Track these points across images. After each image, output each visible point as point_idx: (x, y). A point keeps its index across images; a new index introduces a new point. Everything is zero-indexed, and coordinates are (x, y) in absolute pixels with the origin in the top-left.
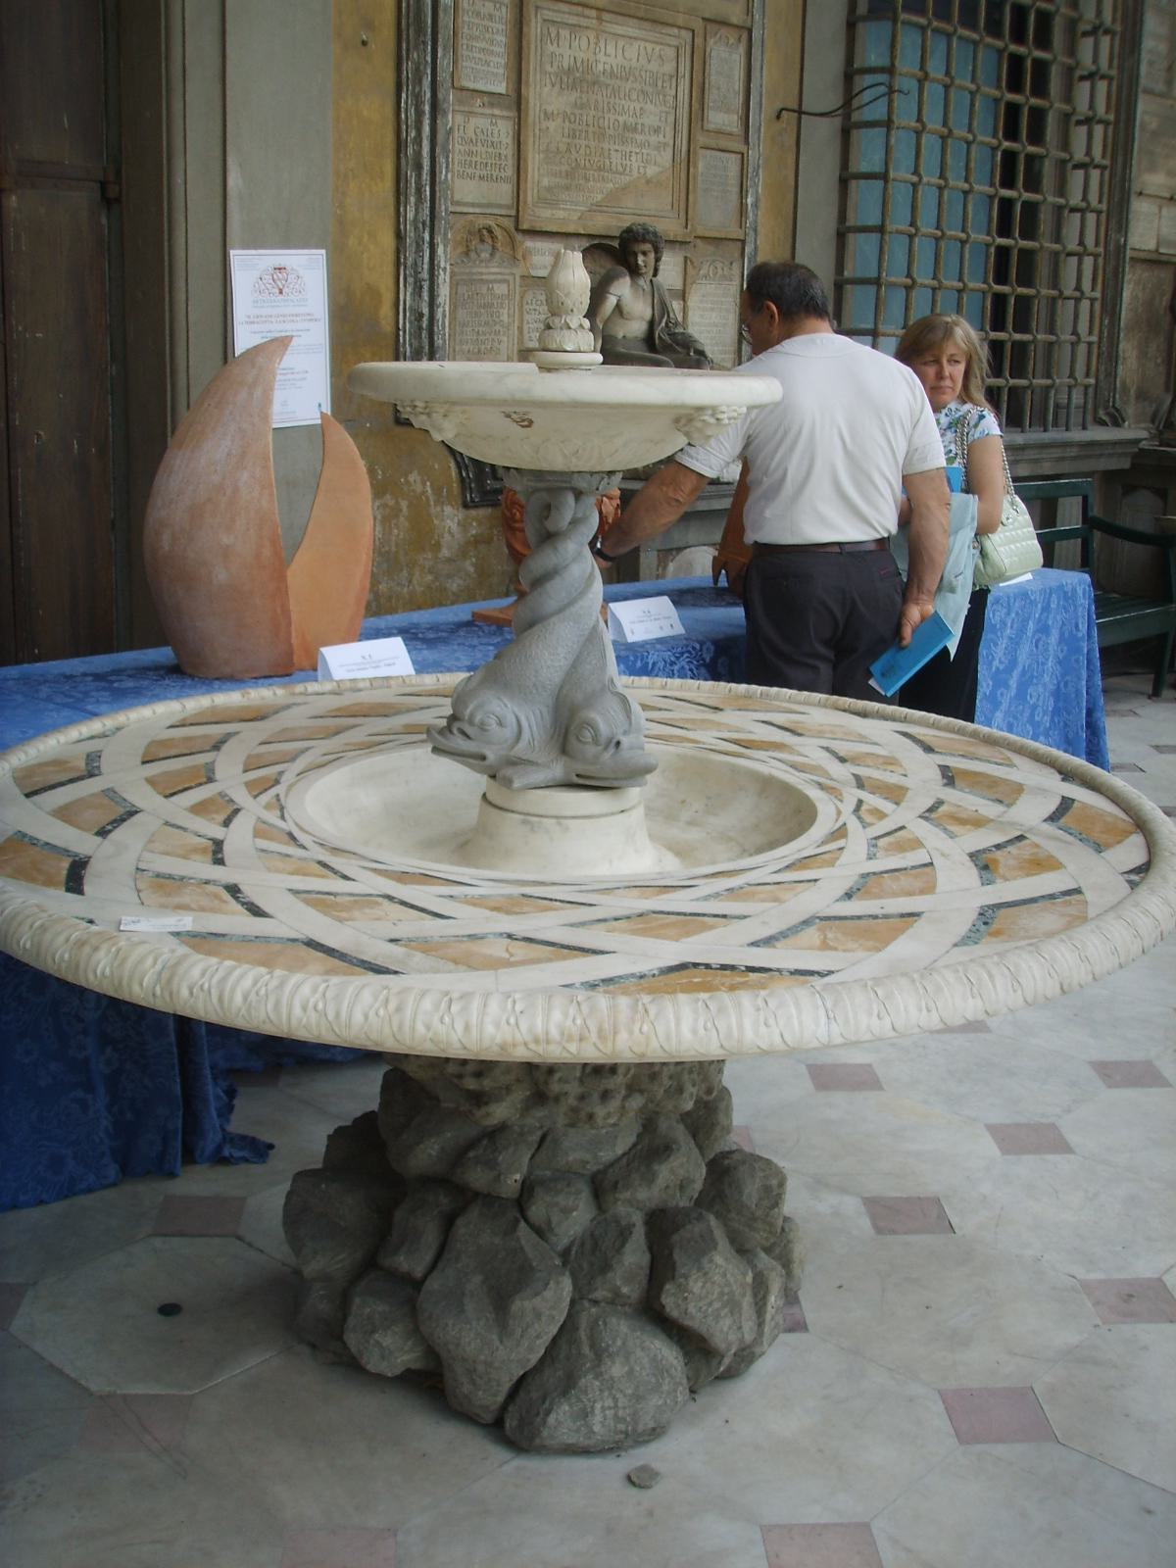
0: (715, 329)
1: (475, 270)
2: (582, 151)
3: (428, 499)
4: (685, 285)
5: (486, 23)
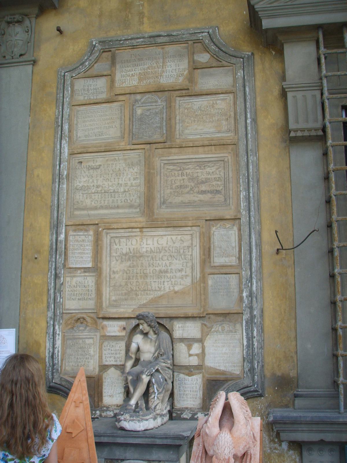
1: (75, 334)
2: (134, 284)
4: (202, 336)
5: (81, 243)
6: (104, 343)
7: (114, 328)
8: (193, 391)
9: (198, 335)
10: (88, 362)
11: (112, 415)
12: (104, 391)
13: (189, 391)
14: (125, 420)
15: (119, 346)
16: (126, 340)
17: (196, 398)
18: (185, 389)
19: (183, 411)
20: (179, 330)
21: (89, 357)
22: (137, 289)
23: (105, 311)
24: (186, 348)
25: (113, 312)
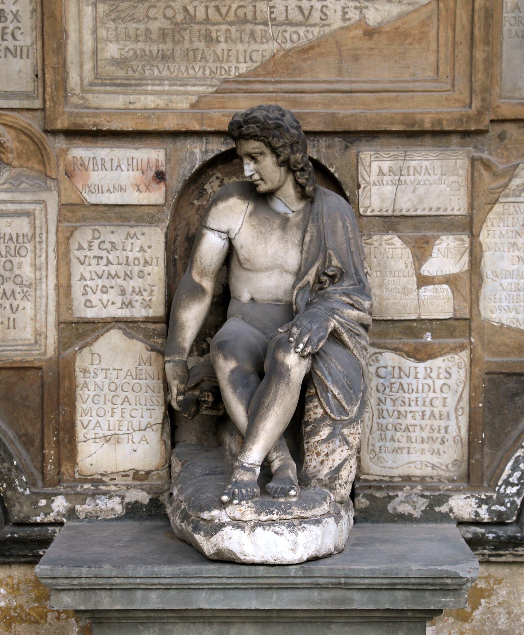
4: (471, 206)
6: (77, 235)
7: (117, 175)
8: (432, 414)
9: (456, 204)
10: (14, 310)
11: (119, 509)
12: (81, 419)
13: (418, 416)
14: (238, 524)
15: (138, 244)
16: (168, 222)
17: (443, 442)
18: (402, 409)
19: (394, 488)
20: (381, 183)
21: (18, 290)
22: (212, 14)
23: (76, 106)
24: (407, 252)
25: (111, 105)
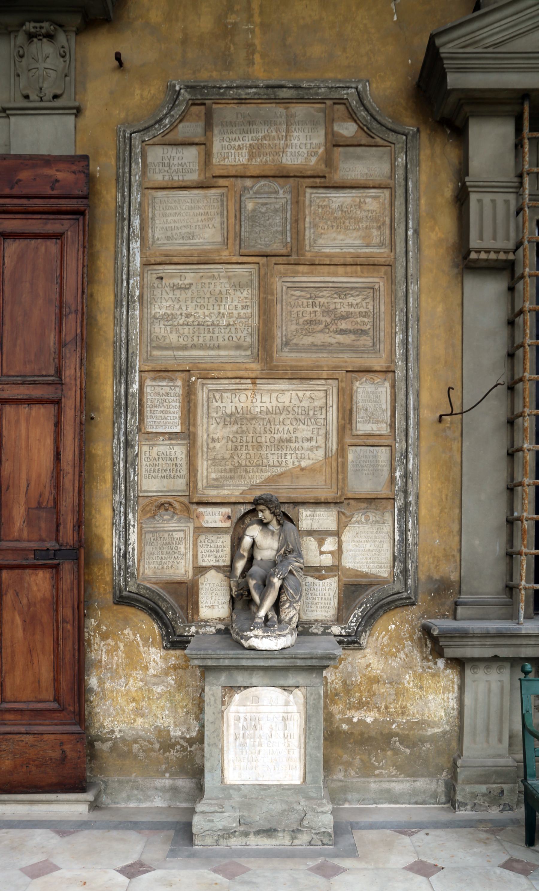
0: (370, 554)
3: (138, 643)
4: (338, 527)
